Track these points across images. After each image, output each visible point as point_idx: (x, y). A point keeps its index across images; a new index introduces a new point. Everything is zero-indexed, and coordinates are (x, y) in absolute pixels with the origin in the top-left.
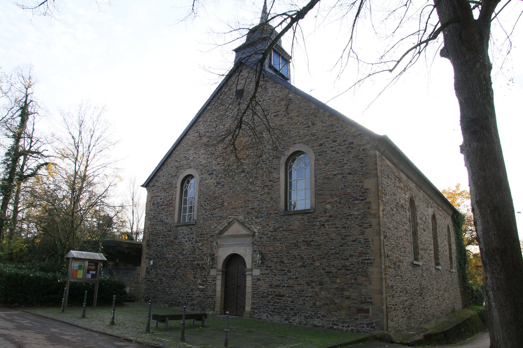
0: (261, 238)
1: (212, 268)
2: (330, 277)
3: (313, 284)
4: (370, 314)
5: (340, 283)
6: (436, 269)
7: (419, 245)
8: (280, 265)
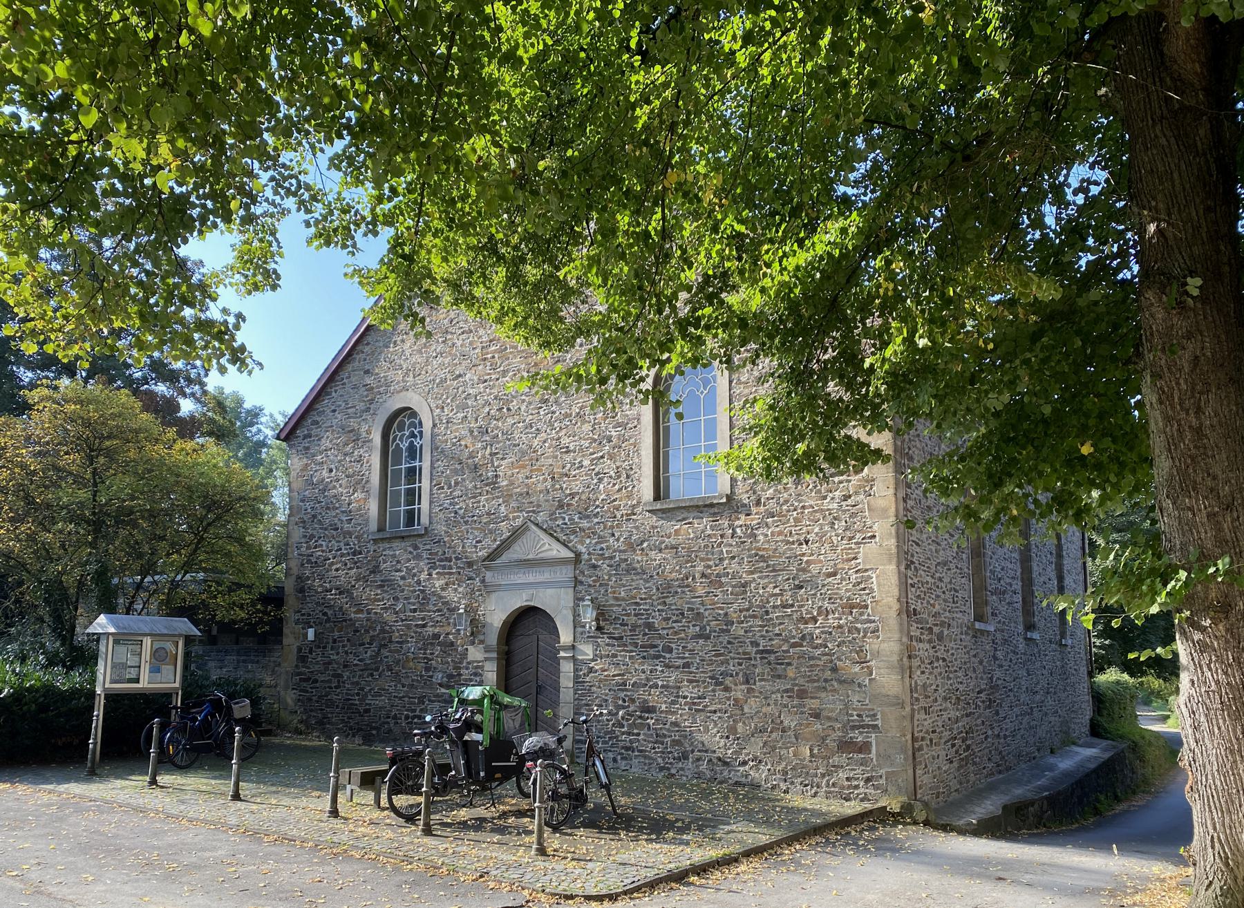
2: (769, 663)
3: (729, 680)
4: (873, 755)
5: (795, 679)
6: (1026, 639)
7: (988, 581)
8: (645, 634)
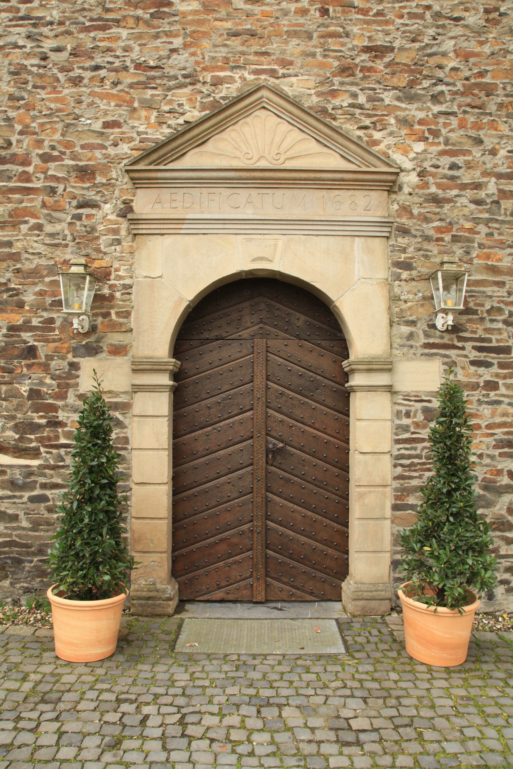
0: (436, 200)
1: (92, 351)
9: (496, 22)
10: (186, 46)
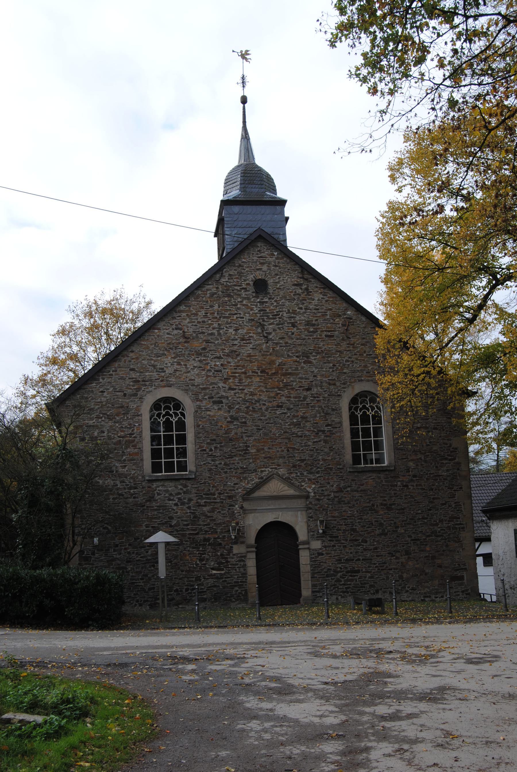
1: (236, 543)
9: (332, 450)
10: (253, 462)
